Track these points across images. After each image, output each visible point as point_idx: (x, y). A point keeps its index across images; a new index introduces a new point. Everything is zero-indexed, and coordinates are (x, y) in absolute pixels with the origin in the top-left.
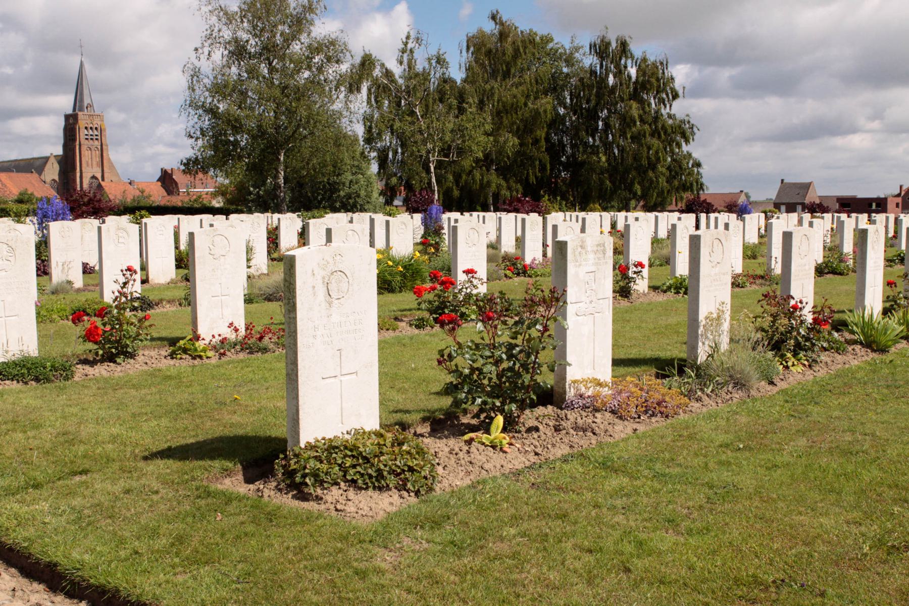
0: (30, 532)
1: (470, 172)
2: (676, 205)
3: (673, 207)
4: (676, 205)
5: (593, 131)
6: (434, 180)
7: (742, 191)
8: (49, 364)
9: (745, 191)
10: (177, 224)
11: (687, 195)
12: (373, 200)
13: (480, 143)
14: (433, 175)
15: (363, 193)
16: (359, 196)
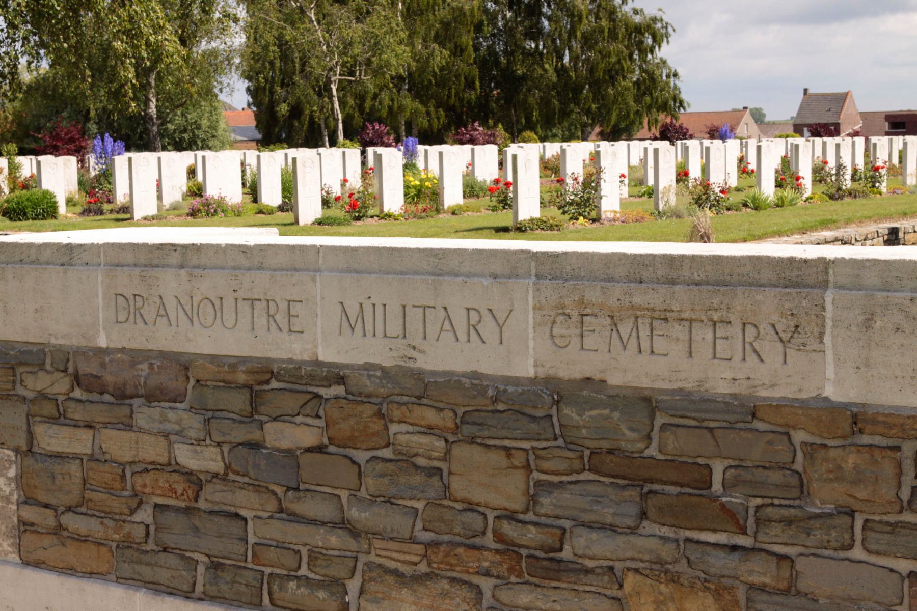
0: (51, 432)
1: (375, 97)
2: (649, 129)
3: (644, 132)
4: (649, 129)
5: (535, 33)
6: (337, 105)
7: (745, 108)
8: (703, 230)
9: (751, 106)
10: (469, 159)
11: (663, 118)
12: (220, 132)
13: (399, 57)
14: (336, 99)
15: (205, 123)
16: (199, 127)
